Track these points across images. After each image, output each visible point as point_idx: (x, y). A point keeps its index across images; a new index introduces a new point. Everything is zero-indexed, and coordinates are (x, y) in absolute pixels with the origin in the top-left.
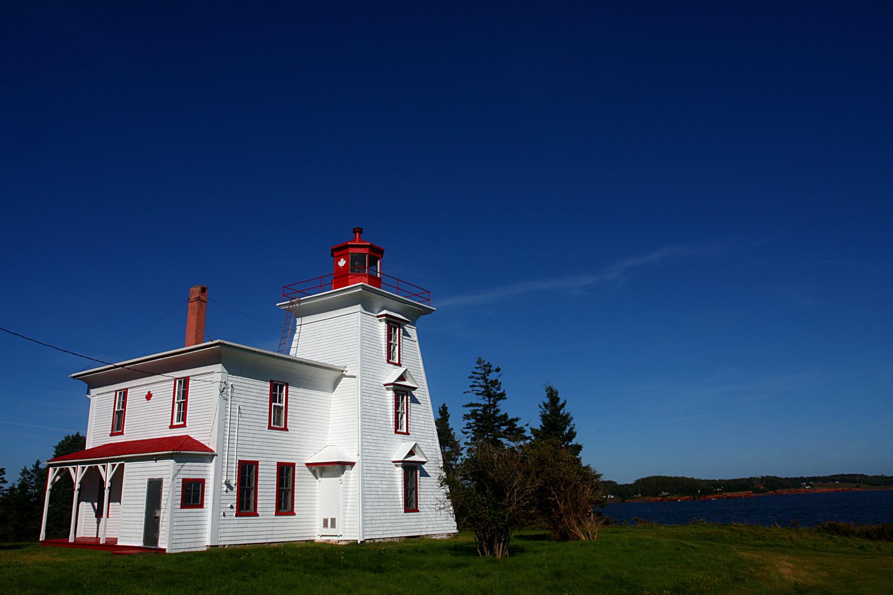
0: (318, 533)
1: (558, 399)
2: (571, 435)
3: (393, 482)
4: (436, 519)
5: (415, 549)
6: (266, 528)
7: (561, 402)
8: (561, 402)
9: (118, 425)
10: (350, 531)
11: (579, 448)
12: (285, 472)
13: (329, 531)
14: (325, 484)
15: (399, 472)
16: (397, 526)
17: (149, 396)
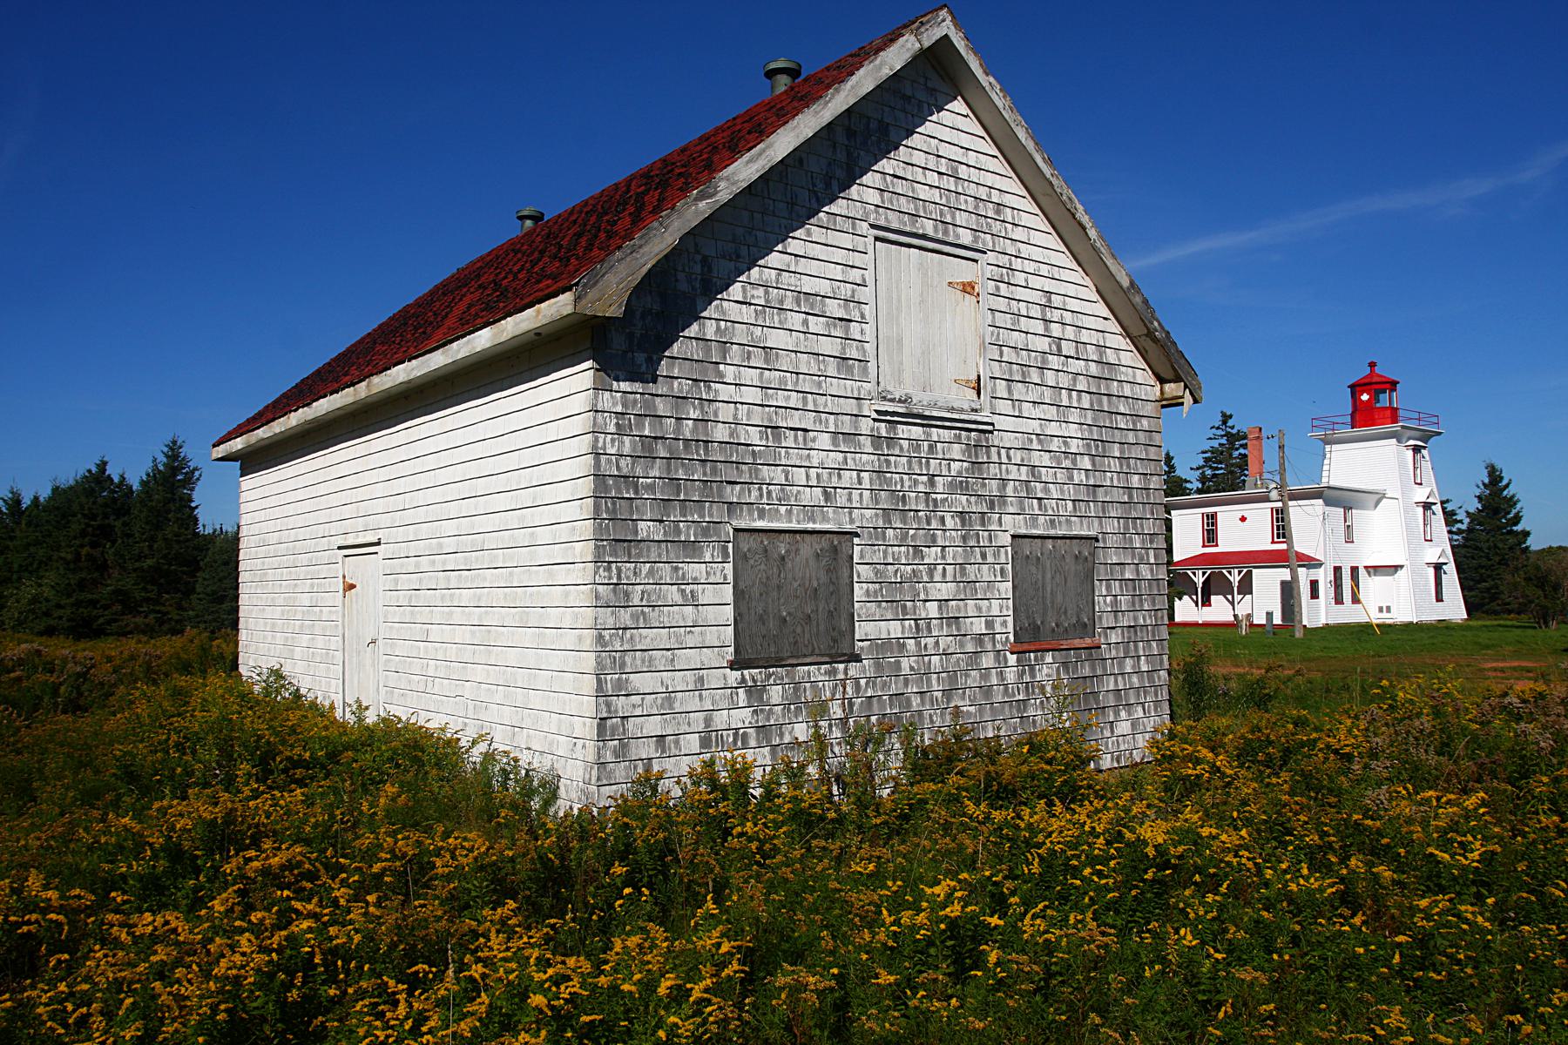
0: (1376, 618)
1: (1502, 478)
2: (1517, 519)
3: (1427, 580)
4: (1454, 609)
5: (1443, 627)
6: (1348, 614)
7: (1504, 482)
8: (1504, 482)
9: (1211, 536)
10: (1404, 613)
11: (1526, 534)
12: (1354, 570)
13: (1385, 615)
14: (1379, 580)
15: (1431, 571)
16: (1432, 613)
17: (1243, 519)
